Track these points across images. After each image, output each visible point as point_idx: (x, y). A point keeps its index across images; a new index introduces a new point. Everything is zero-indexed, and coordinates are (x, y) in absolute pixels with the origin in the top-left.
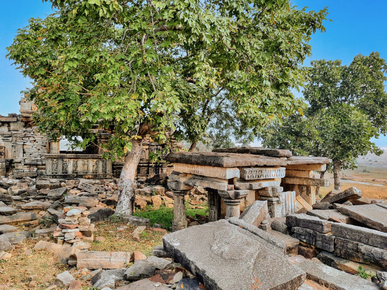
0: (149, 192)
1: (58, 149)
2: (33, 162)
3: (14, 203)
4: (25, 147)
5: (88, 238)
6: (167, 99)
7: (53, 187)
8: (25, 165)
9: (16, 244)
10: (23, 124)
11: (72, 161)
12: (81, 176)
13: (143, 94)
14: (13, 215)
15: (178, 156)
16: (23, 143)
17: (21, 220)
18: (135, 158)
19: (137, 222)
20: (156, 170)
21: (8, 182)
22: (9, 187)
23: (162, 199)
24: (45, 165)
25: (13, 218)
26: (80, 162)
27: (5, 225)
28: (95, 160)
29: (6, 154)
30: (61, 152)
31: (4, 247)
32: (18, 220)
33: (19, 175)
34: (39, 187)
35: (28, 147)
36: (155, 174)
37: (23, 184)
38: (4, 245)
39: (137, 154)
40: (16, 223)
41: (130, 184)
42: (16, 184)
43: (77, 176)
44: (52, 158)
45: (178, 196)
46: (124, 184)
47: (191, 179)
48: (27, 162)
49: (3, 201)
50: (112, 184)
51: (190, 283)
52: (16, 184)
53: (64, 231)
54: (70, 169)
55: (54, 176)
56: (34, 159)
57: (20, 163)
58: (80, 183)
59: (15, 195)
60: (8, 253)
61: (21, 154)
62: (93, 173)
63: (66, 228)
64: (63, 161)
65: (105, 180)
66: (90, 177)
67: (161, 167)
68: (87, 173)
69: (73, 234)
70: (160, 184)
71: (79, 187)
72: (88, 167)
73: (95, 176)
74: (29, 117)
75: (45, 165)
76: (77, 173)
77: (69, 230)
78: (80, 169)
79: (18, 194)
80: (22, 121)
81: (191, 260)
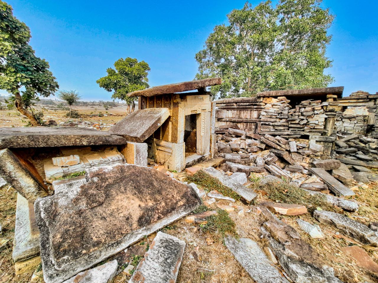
3: (371, 154)
9: (372, 181)
14: (369, 162)
17: (375, 167)
21: (368, 140)
22: (367, 143)
25: (369, 164)
27: (362, 167)
29: (368, 121)
31: (363, 180)
32: (373, 166)
38: (363, 179)
40: (371, 168)
42: (374, 142)
49: (362, 152)
51: (26, 139)
52: (374, 142)
59: (372, 149)
60: (365, 185)
79: (375, 149)
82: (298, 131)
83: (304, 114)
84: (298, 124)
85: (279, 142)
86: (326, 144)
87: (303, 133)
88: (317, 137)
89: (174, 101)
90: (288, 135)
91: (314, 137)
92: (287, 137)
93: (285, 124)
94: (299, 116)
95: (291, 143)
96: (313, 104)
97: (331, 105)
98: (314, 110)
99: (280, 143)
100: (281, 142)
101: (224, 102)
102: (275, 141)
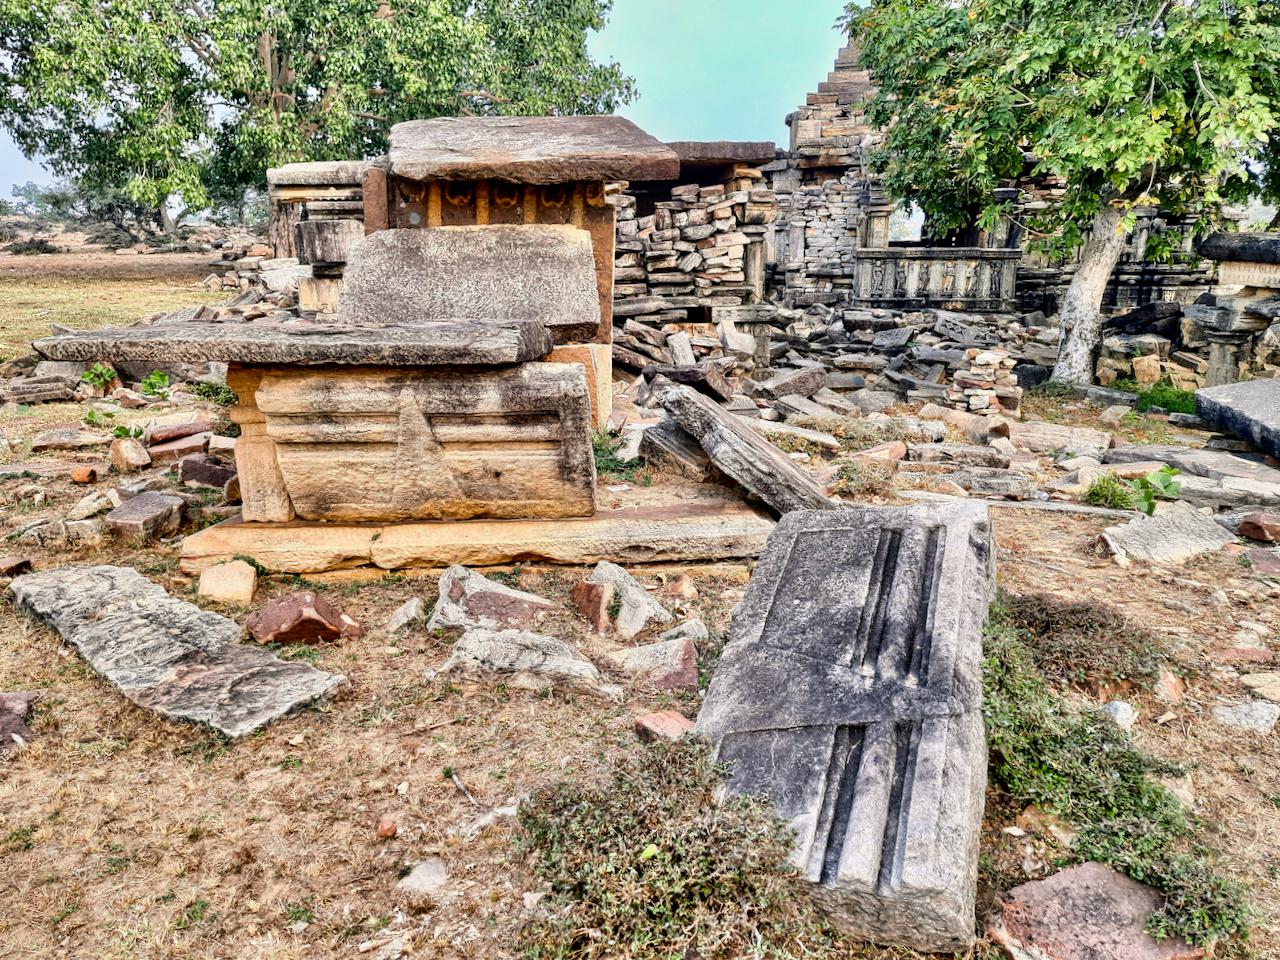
0: (1122, 350)
1: (886, 236)
2: (825, 270)
4: (809, 232)
5: (1011, 412)
6: (1240, 116)
7: (881, 327)
8: (808, 276)
10: (799, 175)
11: (916, 265)
12: (938, 305)
13: (1178, 105)
15: (1236, 243)
16: (803, 224)
18: (1107, 252)
19: (1107, 397)
20: (1140, 292)
23: (1163, 369)
24: (851, 276)
26: (937, 268)
28: (973, 264)
30: (892, 244)
33: (799, 300)
34: (850, 326)
35: (815, 233)
36: (1135, 306)
37: (815, 319)
39: (1114, 242)
41: (1092, 315)
42: (800, 319)
43: (927, 302)
44: (873, 258)
45: (1222, 345)
46: (1077, 313)
47: (1267, 300)
48: (812, 269)
50: (1016, 325)
52: (800, 319)
53: (967, 392)
54: (912, 287)
55: (875, 303)
56: (825, 261)
57: (798, 271)
58: (940, 321)
61: (801, 251)
62: (967, 296)
63: (972, 386)
64: (897, 265)
65: (995, 316)
66: (959, 306)
67: (1159, 283)
68: (951, 296)
69: (987, 400)
70: (1155, 332)
71: (937, 329)
72: (953, 283)
73: (971, 305)
74: (817, 157)
75: (851, 276)
76: (927, 296)
77: (979, 392)
78: (935, 286)
80: (798, 168)
81: (1254, 418)
82: (679, 294)
83: (690, 232)
84: (675, 269)
85: (641, 341)
86: (758, 329)
87: (693, 302)
88: (734, 309)
89: (592, 202)
90: (658, 312)
91: (727, 313)
92: (656, 318)
93: (638, 273)
94: (673, 240)
95: (673, 341)
96: (708, 199)
97: (755, 203)
98: (711, 218)
99: (646, 343)
100: (650, 340)
101: (344, 181)
102: (626, 337)
